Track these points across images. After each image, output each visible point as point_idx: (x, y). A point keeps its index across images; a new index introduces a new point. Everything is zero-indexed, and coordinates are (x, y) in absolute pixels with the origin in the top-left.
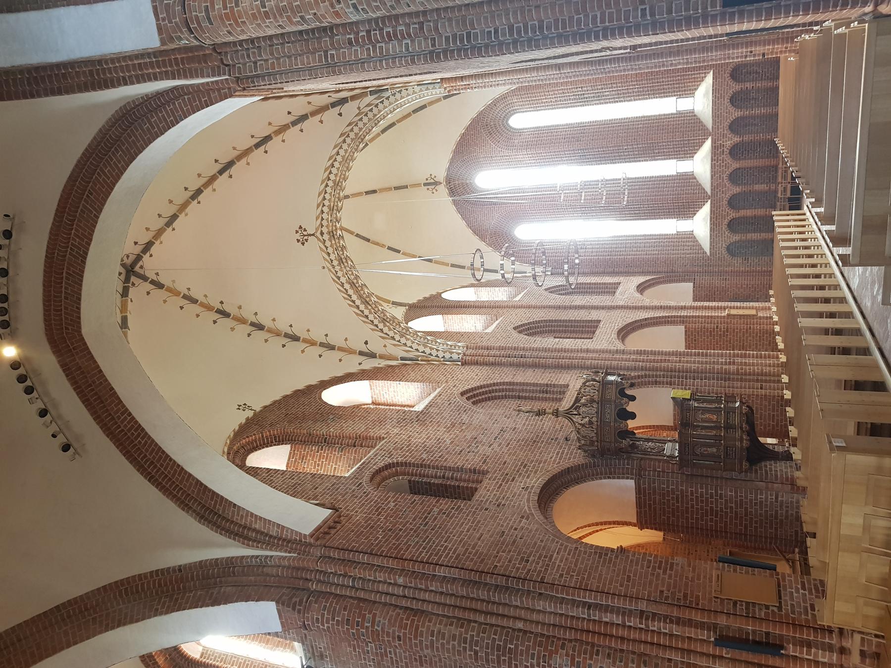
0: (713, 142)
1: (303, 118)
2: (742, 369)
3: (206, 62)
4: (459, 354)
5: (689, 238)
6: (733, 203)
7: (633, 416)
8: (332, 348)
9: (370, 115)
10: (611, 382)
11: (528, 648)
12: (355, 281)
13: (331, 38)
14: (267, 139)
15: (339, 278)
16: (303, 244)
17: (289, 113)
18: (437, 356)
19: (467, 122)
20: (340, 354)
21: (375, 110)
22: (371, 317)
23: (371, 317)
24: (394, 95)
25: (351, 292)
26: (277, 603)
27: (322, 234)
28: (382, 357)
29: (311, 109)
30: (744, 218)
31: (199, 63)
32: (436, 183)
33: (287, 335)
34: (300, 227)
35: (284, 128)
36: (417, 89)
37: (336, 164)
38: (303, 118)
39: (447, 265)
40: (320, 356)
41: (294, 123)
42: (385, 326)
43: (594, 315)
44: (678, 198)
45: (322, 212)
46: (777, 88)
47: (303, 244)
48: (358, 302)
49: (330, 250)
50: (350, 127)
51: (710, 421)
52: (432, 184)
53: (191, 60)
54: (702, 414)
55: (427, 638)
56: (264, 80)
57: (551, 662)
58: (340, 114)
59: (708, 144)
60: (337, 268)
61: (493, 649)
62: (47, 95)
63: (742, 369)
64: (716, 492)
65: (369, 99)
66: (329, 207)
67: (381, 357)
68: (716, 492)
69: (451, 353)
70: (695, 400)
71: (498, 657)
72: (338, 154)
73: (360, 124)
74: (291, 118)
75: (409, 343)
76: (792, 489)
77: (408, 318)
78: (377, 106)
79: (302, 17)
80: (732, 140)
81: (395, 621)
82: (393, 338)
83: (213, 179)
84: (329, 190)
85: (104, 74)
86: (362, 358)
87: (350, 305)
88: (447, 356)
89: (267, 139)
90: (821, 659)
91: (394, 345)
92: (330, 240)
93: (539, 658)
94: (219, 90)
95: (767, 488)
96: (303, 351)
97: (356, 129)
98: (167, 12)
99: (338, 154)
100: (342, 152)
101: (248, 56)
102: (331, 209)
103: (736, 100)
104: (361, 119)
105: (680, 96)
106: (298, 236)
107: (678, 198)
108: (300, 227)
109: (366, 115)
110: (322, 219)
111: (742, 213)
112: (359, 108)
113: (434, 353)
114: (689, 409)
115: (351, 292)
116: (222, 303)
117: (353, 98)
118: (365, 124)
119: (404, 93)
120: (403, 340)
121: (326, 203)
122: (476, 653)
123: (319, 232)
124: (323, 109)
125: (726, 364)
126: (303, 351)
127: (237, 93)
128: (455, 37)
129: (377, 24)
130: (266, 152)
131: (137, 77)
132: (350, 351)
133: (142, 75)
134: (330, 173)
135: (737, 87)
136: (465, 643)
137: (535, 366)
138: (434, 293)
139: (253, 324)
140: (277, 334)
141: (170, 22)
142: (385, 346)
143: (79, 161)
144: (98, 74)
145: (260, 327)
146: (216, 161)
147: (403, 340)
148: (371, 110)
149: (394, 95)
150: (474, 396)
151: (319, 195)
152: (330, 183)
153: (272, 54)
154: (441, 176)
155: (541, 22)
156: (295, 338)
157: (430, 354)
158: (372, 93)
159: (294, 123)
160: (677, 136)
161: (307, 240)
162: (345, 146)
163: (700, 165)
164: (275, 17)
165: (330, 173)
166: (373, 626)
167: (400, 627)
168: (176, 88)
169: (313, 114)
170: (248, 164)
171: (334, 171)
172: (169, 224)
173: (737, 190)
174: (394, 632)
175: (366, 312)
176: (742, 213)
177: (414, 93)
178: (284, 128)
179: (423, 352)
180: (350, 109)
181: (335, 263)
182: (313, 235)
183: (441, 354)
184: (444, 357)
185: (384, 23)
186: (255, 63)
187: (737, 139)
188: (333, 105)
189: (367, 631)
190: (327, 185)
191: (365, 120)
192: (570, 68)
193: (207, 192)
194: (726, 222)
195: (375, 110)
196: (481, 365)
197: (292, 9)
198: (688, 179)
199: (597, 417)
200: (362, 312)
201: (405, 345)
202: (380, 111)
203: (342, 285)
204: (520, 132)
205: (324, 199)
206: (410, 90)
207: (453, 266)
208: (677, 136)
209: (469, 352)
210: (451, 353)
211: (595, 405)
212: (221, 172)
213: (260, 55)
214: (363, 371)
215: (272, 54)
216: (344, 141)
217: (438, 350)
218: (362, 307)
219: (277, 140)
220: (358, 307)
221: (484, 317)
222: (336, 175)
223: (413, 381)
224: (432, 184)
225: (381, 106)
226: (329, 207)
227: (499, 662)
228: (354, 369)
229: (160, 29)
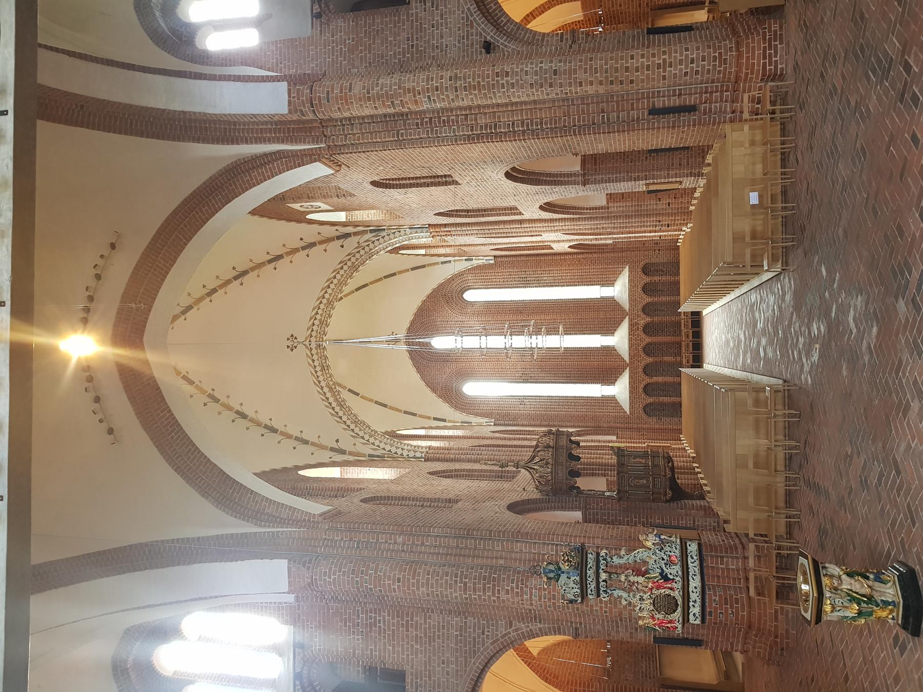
0: (630, 320)
1: (313, 245)
3: (310, 132)
4: (422, 453)
5: (611, 401)
6: (647, 370)
7: (578, 458)
8: (306, 442)
9: (367, 249)
11: (509, 576)
13: (405, 121)
14: (279, 258)
15: (320, 382)
16: (292, 350)
19: (429, 291)
20: (312, 449)
21: (372, 246)
22: (345, 418)
23: (345, 418)
24: (388, 235)
25: (329, 395)
26: (289, 560)
28: (351, 453)
29: (320, 238)
30: (656, 383)
31: (306, 132)
33: (266, 427)
34: (292, 336)
35: (294, 251)
37: (332, 286)
38: (313, 245)
39: (400, 411)
40: (294, 448)
41: (304, 248)
44: (600, 367)
45: (313, 324)
46: (679, 282)
47: (292, 350)
48: (334, 404)
49: (315, 357)
51: (641, 463)
53: (299, 130)
55: (423, 576)
56: (348, 148)
57: (528, 584)
58: (342, 246)
59: (627, 319)
60: (319, 373)
61: (480, 579)
62: (189, 141)
64: (647, 520)
65: (368, 236)
66: (320, 320)
67: (351, 453)
68: (647, 520)
71: (484, 585)
72: (335, 277)
73: (358, 256)
74: (303, 244)
75: (377, 443)
76: (705, 514)
78: (373, 242)
79: (392, 102)
80: (644, 320)
81: (396, 567)
82: (363, 438)
83: (228, 282)
84: (322, 306)
85: (234, 132)
88: (412, 454)
89: (279, 258)
90: (731, 567)
91: (363, 444)
92: (316, 348)
93: (518, 582)
94: (310, 155)
95: (686, 515)
96: (279, 442)
97: (353, 259)
98: (298, 93)
99: (335, 277)
100: (338, 277)
101: (343, 130)
102: (321, 322)
103: (647, 289)
104: (359, 252)
105: (603, 285)
106: (290, 343)
107: (600, 367)
108: (292, 336)
110: (312, 330)
111: (655, 379)
113: (399, 452)
115: (329, 395)
116: (213, 390)
117: (355, 234)
118: (361, 256)
119: (397, 234)
120: (372, 440)
121: (318, 317)
122: (465, 584)
126: (279, 442)
127: (323, 160)
128: (486, 126)
129: (438, 113)
130: (275, 269)
131: (256, 139)
133: (260, 138)
134: (326, 292)
135: (647, 279)
136: (456, 577)
139: (238, 412)
140: (259, 424)
141: (298, 99)
142: (355, 444)
143: (185, 199)
144: (230, 132)
145: (243, 416)
146: (234, 268)
147: (372, 440)
148: (368, 245)
149: (388, 235)
152: (325, 301)
153: (361, 129)
155: (541, 119)
156: (274, 431)
157: (396, 453)
159: (304, 248)
160: (600, 316)
161: (296, 347)
162: (342, 272)
163: (619, 340)
164: (374, 101)
165: (326, 292)
166: (376, 573)
167: (400, 571)
168: (279, 152)
169: (321, 243)
170: (258, 276)
171: (329, 291)
172: (184, 312)
173: (650, 360)
174: (395, 575)
175: (341, 413)
176: (655, 379)
177: (405, 234)
178: (294, 251)
179: (390, 451)
180: (353, 241)
181: (318, 369)
185: (443, 113)
186: (346, 136)
187: (648, 319)
188: (338, 238)
189: (370, 578)
190: (321, 302)
191: (362, 252)
193: (221, 292)
194: (642, 386)
195: (372, 246)
197: (387, 96)
198: (608, 351)
200: (337, 413)
201: (373, 444)
202: (375, 247)
203: (322, 388)
204: (472, 304)
205: (317, 313)
206: (402, 233)
207: (406, 412)
208: (600, 316)
209: (431, 451)
211: (550, 450)
212: (236, 278)
213: (352, 130)
215: (361, 129)
216: (342, 268)
217: (403, 449)
218: (337, 409)
219: (287, 259)
220: (333, 408)
222: (330, 295)
226: (320, 320)
227: (484, 589)
228: (327, 460)
229: (290, 103)
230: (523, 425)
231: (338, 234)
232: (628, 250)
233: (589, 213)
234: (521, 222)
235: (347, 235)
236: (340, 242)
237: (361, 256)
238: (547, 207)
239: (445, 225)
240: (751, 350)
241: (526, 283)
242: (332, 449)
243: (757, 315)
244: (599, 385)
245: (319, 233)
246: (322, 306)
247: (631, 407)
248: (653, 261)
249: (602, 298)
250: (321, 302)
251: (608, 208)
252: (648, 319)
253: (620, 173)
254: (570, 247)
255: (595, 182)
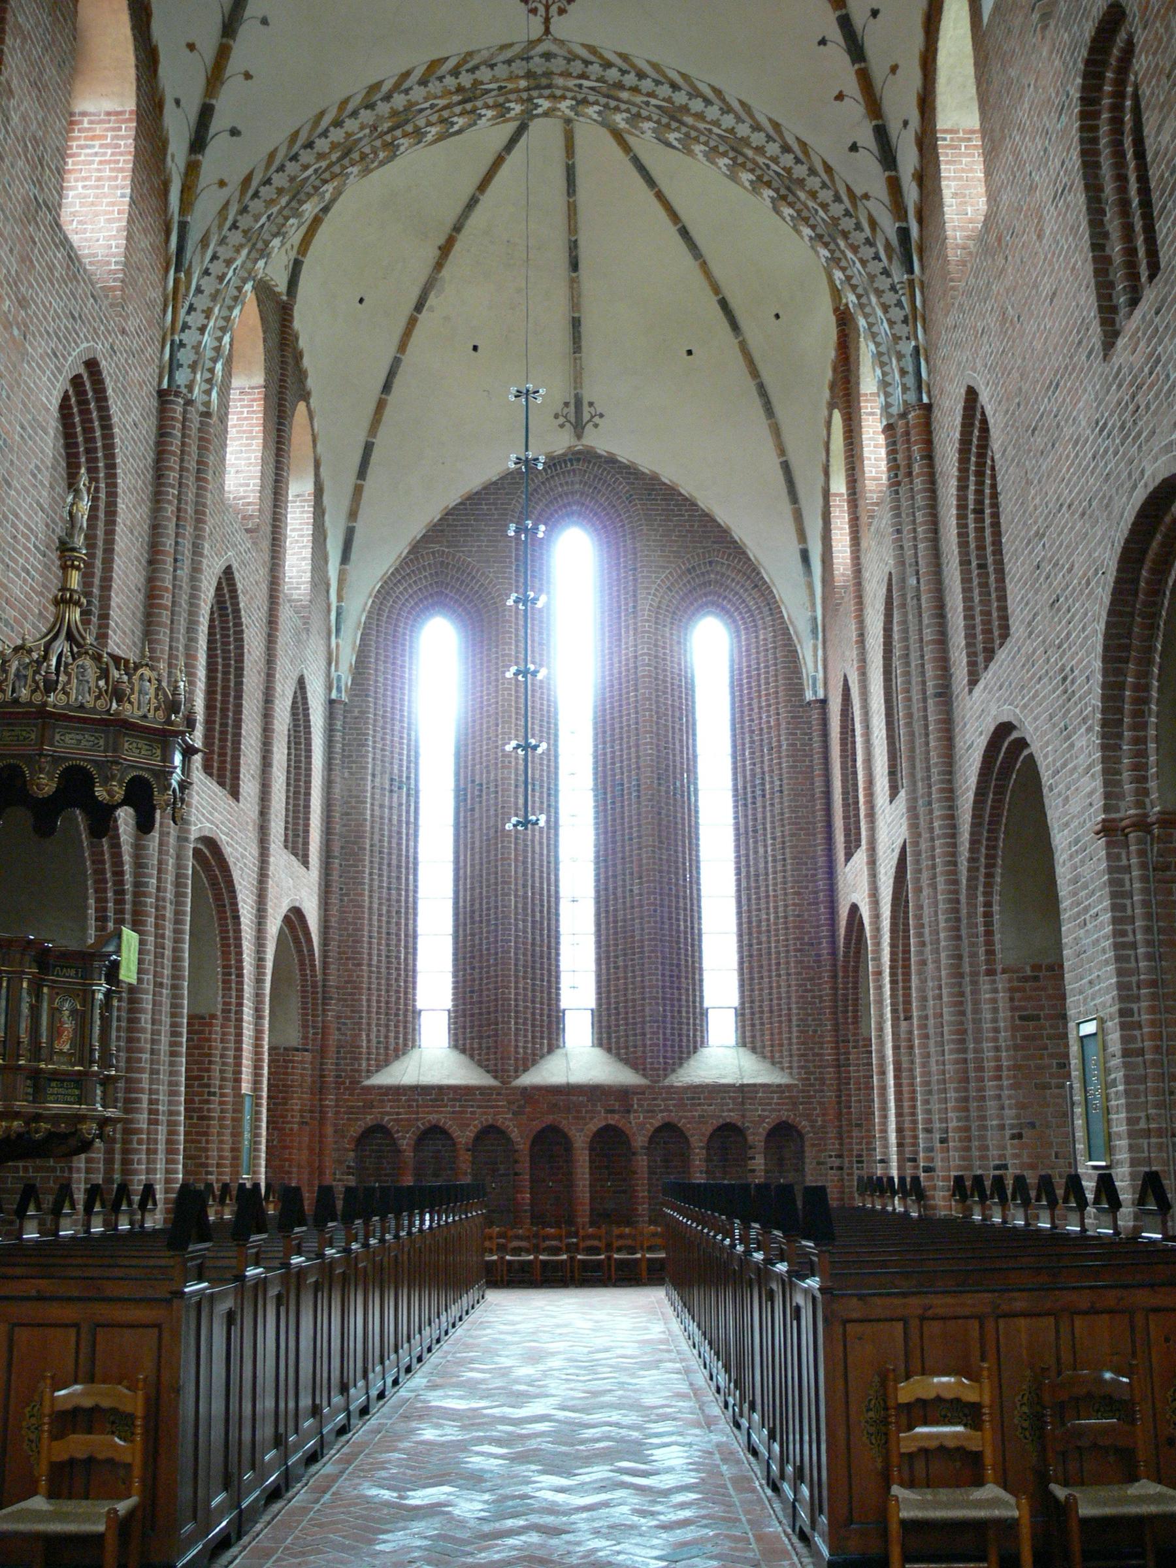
1: (856, 50)
2: (140, 1142)
4: (190, 388)
5: (401, 1031)
10: (167, 758)
12: (409, 128)
17: (875, 13)
18: (186, 326)
19: (722, 516)
24: (893, 288)
27: (547, 56)
28: (192, 168)
29: (879, 71)
32: (579, 428)
36: (907, 348)
38: (856, 50)
42: (334, 146)
43: (249, 786)
50: (820, 168)
51: (55, 1032)
52: (577, 415)
54: (73, 1012)
63: (140, 1142)
65: (889, 226)
67: (192, 168)
69: (193, 367)
70: (108, 995)
73: (826, 195)
77: (264, 290)
78: (869, 242)
80: (640, 1128)
86: (192, 109)
87: (346, 102)
100: (758, 139)
103: (728, 1137)
104: (838, 199)
105: (740, 1014)
109: (847, 213)
112: (866, 196)
113: (195, 320)
114: (87, 975)
117: (894, 186)
123: (554, 48)
124: (874, 106)
125: (151, 1102)
132: (215, 77)
135: (757, 1137)
137: (151, 593)
138: (310, 383)
142: (222, 184)
150: (83, 403)
151: (655, 66)
152: (680, 98)
154: (599, 440)
158: (904, 234)
162: (773, 149)
163: (579, 1056)
169: (865, 79)
180: (866, 175)
182: (547, 31)
183: (189, 337)
184: (182, 345)
187: (640, 1141)
188: (881, 133)
191: (837, 210)
192: (938, 721)
195: (858, 238)
196: (159, 443)
198: (548, 1030)
199: (68, 706)
202: (855, 249)
207: (368, 448)
210: (193, 367)
214: (159, 106)
221: (253, 497)
223: (129, 238)
224: (577, 415)
225: (867, 252)
230: (328, 784)
231: (894, 127)
232: (842, 1082)
233: (971, 915)
234: (945, 694)
235: (888, 158)
236: (866, 137)
237: (824, 206)
238: (1008, 753)
239: (929, 457)
240: (462, 1447)
241: (747, 796)
242: (206, 113)
243: (599, 1472)
244: (448, 1004)
245: (894, 69)
246: (664, 90)
247: (373, 1087)
248: (810, 1153)
249: (704, 1014)
250: (675, 87)
251: (991, 972)
252: (640, 1141)
253: (1149, 957)
254: (854, 908)
255: (1116, 870)
